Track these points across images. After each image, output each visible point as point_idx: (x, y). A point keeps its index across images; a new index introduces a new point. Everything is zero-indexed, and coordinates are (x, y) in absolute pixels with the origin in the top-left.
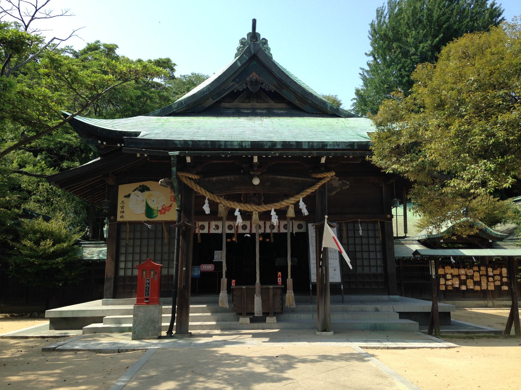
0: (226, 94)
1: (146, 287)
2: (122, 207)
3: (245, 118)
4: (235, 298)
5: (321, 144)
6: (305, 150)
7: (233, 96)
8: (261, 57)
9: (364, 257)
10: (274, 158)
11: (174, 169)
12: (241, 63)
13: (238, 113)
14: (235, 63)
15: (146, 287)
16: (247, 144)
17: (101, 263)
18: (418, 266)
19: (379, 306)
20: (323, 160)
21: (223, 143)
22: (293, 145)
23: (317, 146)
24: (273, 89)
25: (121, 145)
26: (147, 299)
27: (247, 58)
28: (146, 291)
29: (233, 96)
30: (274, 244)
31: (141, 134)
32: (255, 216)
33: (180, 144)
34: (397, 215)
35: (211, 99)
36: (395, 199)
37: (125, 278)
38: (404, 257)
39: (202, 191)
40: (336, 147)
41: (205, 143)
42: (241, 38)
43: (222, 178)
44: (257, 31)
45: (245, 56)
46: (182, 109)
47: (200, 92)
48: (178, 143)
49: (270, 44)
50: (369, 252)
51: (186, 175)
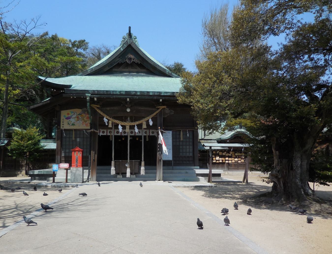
0: (115, 64)
1: (76, 160)
2: (63, 122)
3: (125, 77)
6: (151, 96)
7: (119, 65)
8: (133, 46)
11: (88, 104)
12: (123, 48)
15: (76, 160)
17: (53, 150)
19: (187, 171)
20: (161, 100)
26: (77, 165)
27: (126, 46)
28: (76, 161)
30: (136, 140)
31: (72, 87)
32: (128, 127)
35: (107, 67)
42: (123, 36)
43: (112, 108)
44: (131, 32)
46: (93, 72)
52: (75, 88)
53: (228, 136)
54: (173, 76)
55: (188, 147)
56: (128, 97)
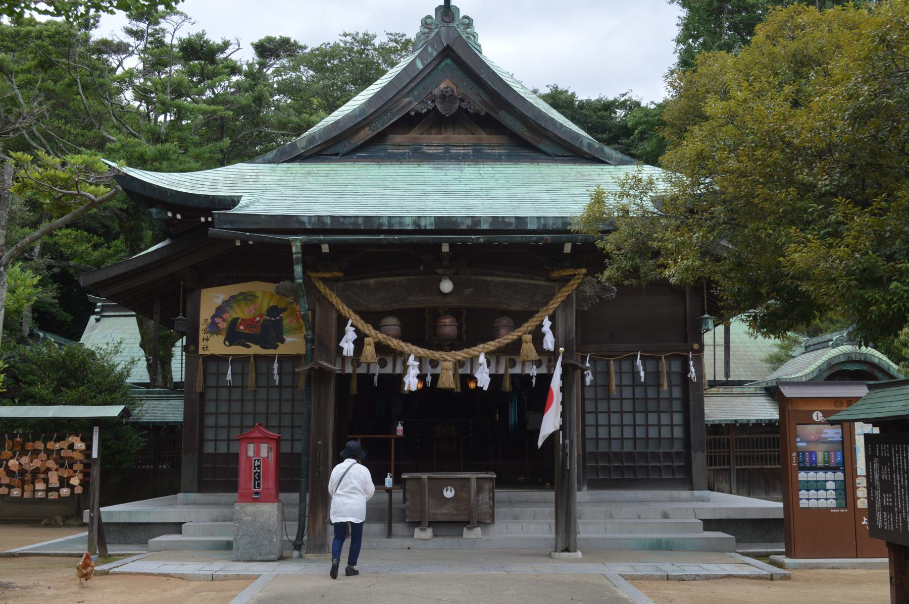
1: (255, 473)
4: (407, 495)
5: (560, 221)
7: (408, 122)
8: (460, 52)
9: (662, 422)
10: (476, 246)
11: (298, 269)
15: (255, 473)
16: (428, 222)
18: (764, 436)
20: (568, 248)
21: (385, 221)
22: (510, 224)
23: (554, 224)
25: (206, 219)
27: (435, 54)
29: (408, 122)
31: (243, 202)
33: (309, 222)
36: (707, 316)
37: (215, 456)
38: (736, 421)
39: (345, 311)
41: (353, 220)
45: (430, 49)
46: (315, 150)
47: (347, 117)
48: (306, 220)
49: (477, 28)
50: (621, 412)
51: (320, 275)
52: (250, 211)
53: (807, 371)
54: (611, 158)
55: (665, 419)
56: (445, 241)
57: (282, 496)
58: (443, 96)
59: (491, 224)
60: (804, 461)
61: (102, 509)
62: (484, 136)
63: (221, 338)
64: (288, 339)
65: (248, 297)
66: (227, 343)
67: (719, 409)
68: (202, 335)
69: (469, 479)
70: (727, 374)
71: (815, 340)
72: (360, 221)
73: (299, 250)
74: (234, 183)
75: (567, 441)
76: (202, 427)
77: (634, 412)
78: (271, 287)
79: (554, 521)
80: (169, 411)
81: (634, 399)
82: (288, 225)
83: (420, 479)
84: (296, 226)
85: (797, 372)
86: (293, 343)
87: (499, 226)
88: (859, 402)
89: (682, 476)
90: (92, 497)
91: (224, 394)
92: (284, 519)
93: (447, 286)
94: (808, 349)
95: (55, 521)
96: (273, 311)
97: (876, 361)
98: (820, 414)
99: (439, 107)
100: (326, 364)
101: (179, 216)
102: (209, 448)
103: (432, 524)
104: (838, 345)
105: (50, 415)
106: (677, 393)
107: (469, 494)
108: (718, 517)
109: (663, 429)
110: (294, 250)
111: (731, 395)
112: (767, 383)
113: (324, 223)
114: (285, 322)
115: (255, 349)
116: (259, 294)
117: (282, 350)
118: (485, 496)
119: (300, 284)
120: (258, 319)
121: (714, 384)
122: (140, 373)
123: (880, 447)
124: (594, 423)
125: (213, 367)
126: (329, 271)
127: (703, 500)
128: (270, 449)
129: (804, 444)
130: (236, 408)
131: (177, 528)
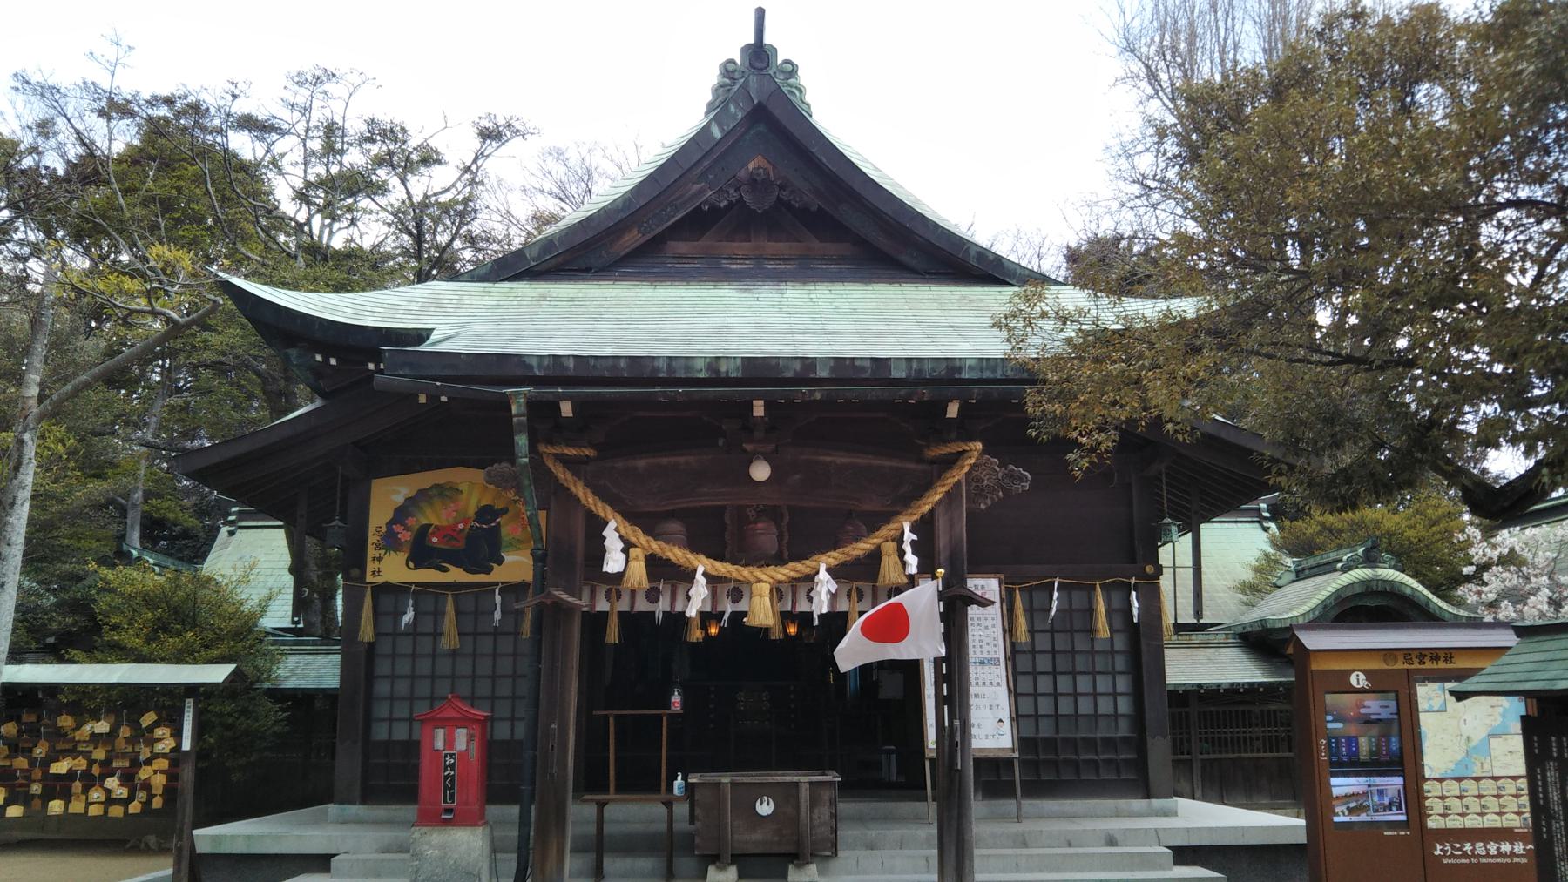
4: (698, 811)
5: (944, 365)
6: (899, 382)
7: (699, 222)
8: (777, 112)
10: (809, 405)
11: (522, 441)
12: (722, 130)
13: (714, 271)
14: (704, 131)
15: (446, 777)
16: (732, 366)
20: (953, 410)
21: (663, 365)
22: (863, 369)
24: (815, 204)
27: (740, 116)
28: (446, 787)
29: (699, 222)
31: (434, 337)
33: (540, 366)
34: (1174, 567)
36: (1167, 520)
37: (389, 744)
38: (1200, 685)
39: (601, 509)
40: (987, 374)
41: (610, 362)
42: (723, 60)
43: (664, 461)
44: (767, 40)
45: (732, 109)
46: (553, 262)
48: (534, 362)
49: (804, 78)
51: (557, 450)
53: (1306, 608)
55: (1103, 684)
57: (493, 811)
58: (753, 181)
59: (833, 369)
60: (1337, 752)
61: (195, 832)
62: (816, 244)
63: (402, 557)
64: (509, 558)
65: (445, 492)
66: (411, 565)
67: (1187, 668)
68: (371, 552)
69: (796, 784)
70: (1198, 613)
71: (1311, 562)
72: (622, 364)
73: (523, 410)
74: (423, 309)
75: (957, 722)
76: (369, 698)
77: (1054, 674)
78: (479, 475)
79: (935, 852)
80: (316, 670)
81: (1054, 652)
82: (502, 370)
83: (718, 784)
84: (519, 372)
85: (1291, 610)
86: (516, 565)
87: (846, 371)
88: (1505, 659)
89: (1136, 780)
90: (179, 817)
91: (405, 646)
92: (495, 849)
93: (761, 472)
94: (1300, 575)
95: (147, 845)
96: (486, 513)
97: (1408, 591)
98: (1362, 676)
99: (746, 198)
100: (565, 596)
101: (333, 361)
102: (380, 733)
103: (736, 859)
104: (1350, 569)
105: (114, 679)
106: (1120, 643)
107: (798, 808)
108: (1195, 842)
109: (1081, 700)
110: (514, 410)
111: (1189, 645)
112: (1244, 626)
113: (562, 366)
114: (504, 531)
115: (456, 574)
116: (464, 487)
117: (498, 574)
118: (824, 812)
119: (525, 465)
120: (461, 526)
121: (1179, 628)
122: (279, 615)
123: (1559, 743)
124: (1031, 691)
125: (387, 602)
126: (573, 446)
127: (1166, 813)
128: (470, 738)
129: (1340, 725)
130: (484, 667)
131: (321, 862)
